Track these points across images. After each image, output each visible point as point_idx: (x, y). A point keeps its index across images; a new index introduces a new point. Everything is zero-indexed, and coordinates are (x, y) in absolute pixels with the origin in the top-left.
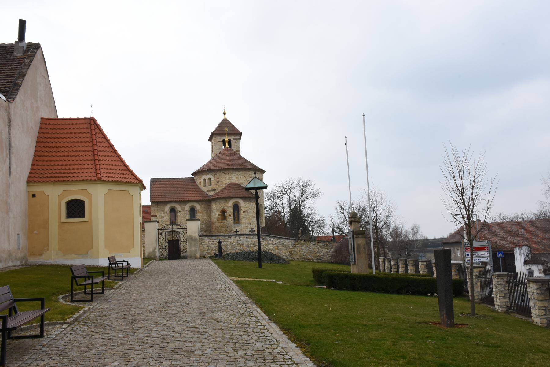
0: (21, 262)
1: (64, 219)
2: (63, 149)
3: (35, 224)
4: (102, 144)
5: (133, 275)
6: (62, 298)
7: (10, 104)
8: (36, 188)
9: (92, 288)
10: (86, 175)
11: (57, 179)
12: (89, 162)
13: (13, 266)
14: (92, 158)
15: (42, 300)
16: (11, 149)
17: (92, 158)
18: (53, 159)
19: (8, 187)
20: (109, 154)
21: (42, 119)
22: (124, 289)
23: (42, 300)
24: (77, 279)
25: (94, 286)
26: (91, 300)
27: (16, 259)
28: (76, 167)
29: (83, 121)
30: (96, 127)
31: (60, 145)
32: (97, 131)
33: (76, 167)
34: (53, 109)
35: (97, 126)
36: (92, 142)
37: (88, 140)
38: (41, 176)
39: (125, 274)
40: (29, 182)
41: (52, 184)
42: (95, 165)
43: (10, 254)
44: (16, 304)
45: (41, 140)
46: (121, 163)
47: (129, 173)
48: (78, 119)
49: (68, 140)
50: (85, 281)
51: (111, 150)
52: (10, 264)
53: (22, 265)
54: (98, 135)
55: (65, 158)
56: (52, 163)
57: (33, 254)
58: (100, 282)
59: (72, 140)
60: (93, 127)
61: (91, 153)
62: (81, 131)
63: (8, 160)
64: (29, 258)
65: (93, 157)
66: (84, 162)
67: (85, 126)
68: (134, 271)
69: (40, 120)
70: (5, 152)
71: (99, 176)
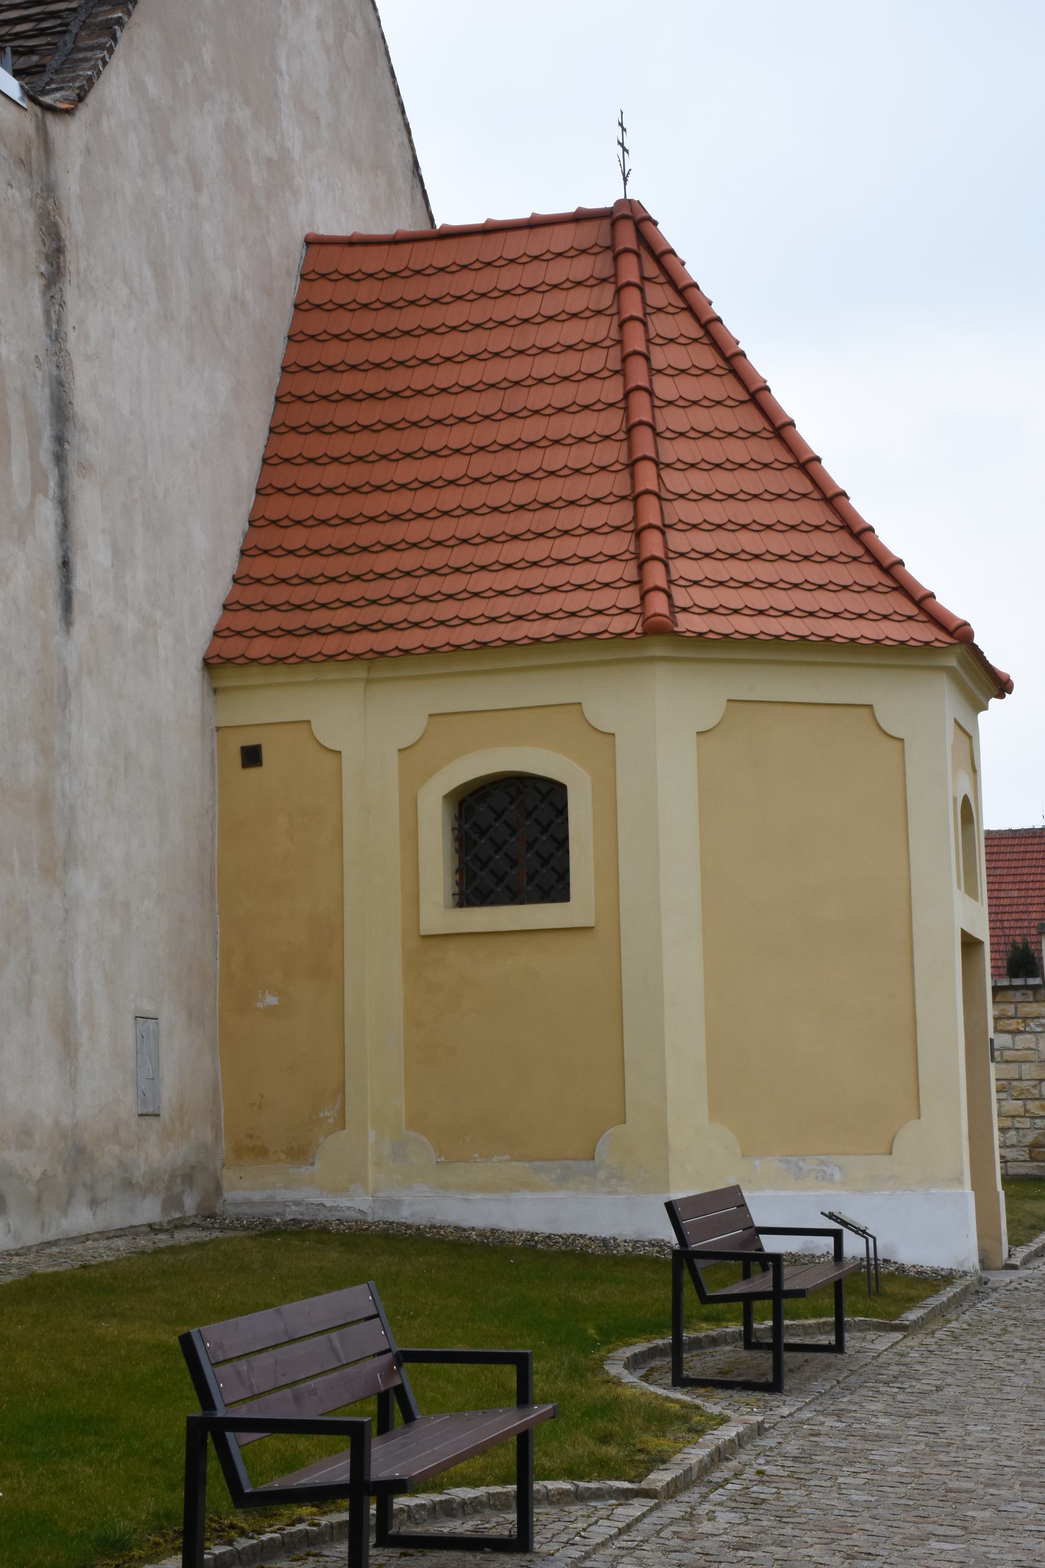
0: (172, 1201)
1: (438, 912)
2: (435, 438)
3: (259, 949)
4: (690, 388)
5: (885, 1341)
6: (633, 1363)
7: (55, 126)
8: (267, 706)
9: (777, 1319)
10: (576, 601)
11: (386, 641)
12: (595, 516)
13: (106, 1235)
14: (618, 484)
15: (521, 1362)
16: (74, 437)
17: (618, 484)
18: (375, 504)
19: (57, 695)
20: (737, 451)
21: (312, 242)
22: (733, 1504)
23: (521, 1362)
24: (700, 1263)
25: (787, 1303)
26: (775, 1387)
27: (128, 1184)
28: (513, 552)
29: (563, 239)
30: (651, 269)
31: (417, 409)
32: (659, 295)
33: (513, 552)
34: (403, 180)
35: (661, 258)
36: (622, 372)
37: (593, 361)
38: (294, 620)
39: (805, 1326)
40: (221, 664)
41: (359, 671)
42: (638, 533)
43: (80, 1150)
44: (409, 1375)
45: (306, 384)
46: (815, 513)
47: (870, 576)
48: (535, 224)
49: (470, 373)
50: (747, 1275)
51: (750, 419)
52: (81, 1219)
53: (178, 1225)
54: (661, 325)
55: (449, 498)
56: (367, 535)
57: (252, 1150)
58: (818, 1289)
59: (495, 371)
60: (629, 270)
61: (611, 453)
62: (554, 303)
63: (47, 512)
64: (228, 1177)
65: (624, 478)
66: (567, 519)
67: (581, 268)
68: (911, 1302)
69: (298, 251)
70: (24, 458)
71: (658, 604)
